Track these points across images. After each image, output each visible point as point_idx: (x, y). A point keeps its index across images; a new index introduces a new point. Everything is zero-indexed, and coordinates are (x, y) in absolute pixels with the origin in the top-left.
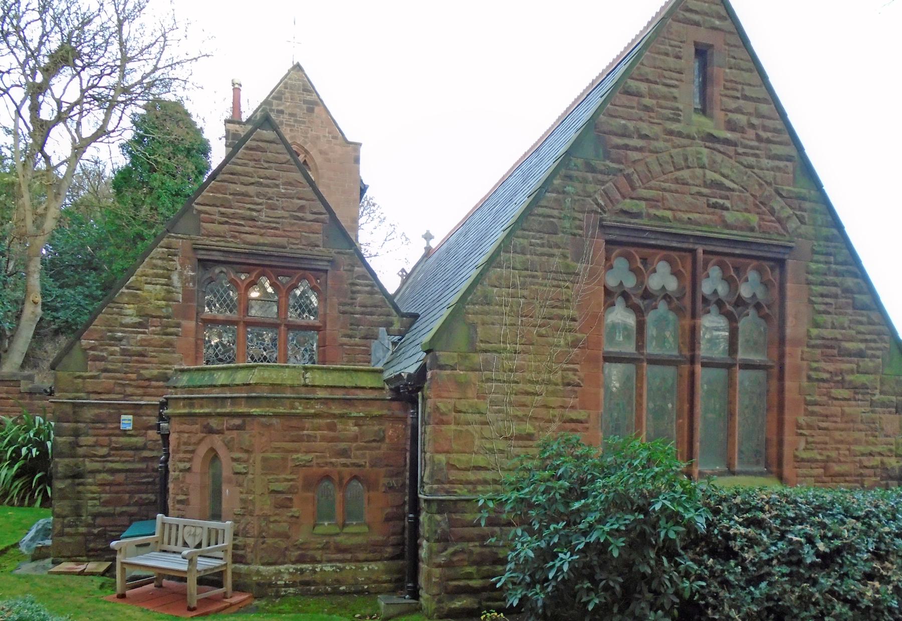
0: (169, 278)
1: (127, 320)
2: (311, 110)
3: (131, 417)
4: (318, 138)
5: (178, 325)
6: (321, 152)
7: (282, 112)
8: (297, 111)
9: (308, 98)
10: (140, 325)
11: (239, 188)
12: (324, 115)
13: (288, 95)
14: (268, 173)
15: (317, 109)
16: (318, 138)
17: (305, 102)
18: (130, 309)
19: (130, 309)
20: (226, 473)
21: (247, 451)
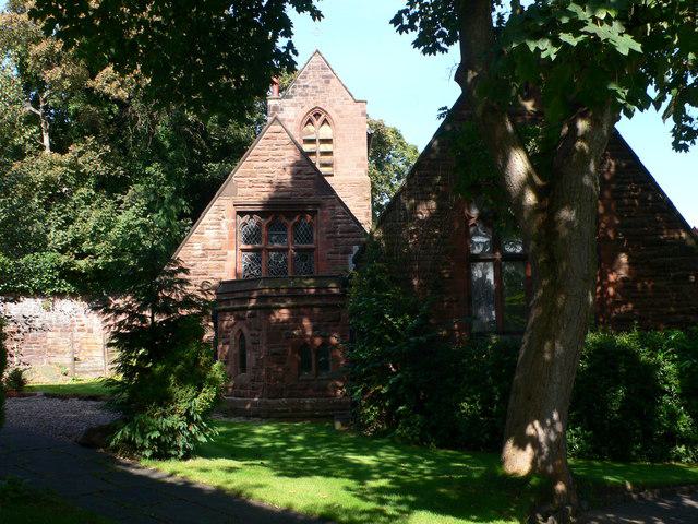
0: (219, 224)
1: (196, 253)
2: (328, 82)
3: (41, 375)
4: (334, 101)
5: (226, 254)
6: (336, 111)
7: (307, 86)
8: (318, 84)
9: (325, 74)
10: (204, 255)
11: (260, 164)
12: (338, 84)
13: (311, 74)
14: (277, 152)
15: (332, 81)
16: (334, 101)
17: (323, 77)
18: (197, 246)
19: (197, 246)
20: (248, 343)
21: (259, 330)
